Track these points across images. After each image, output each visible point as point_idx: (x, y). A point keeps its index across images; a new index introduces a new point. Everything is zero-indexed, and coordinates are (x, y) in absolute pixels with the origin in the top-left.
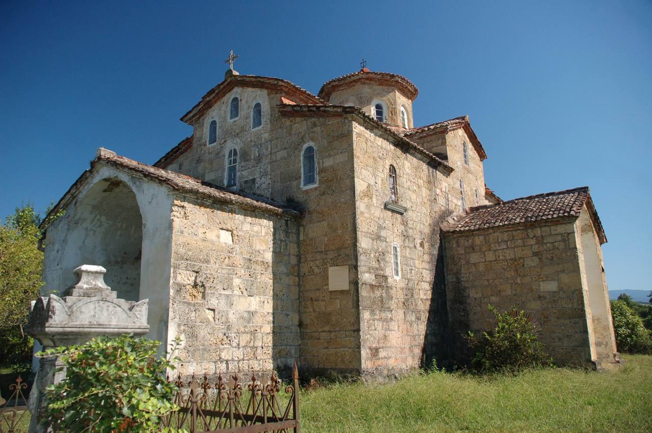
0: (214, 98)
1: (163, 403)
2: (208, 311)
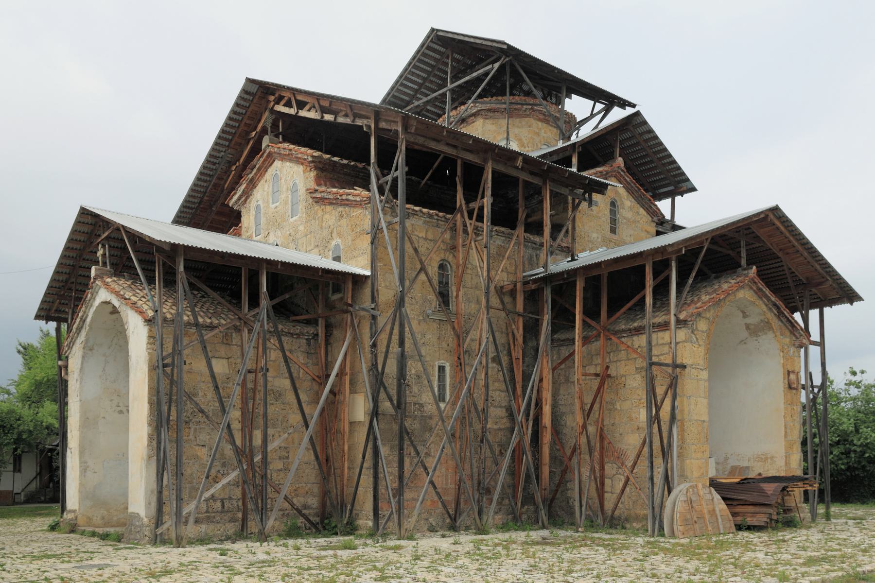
0: (256, 174)
1: (710, 492)
2: (197, 448)
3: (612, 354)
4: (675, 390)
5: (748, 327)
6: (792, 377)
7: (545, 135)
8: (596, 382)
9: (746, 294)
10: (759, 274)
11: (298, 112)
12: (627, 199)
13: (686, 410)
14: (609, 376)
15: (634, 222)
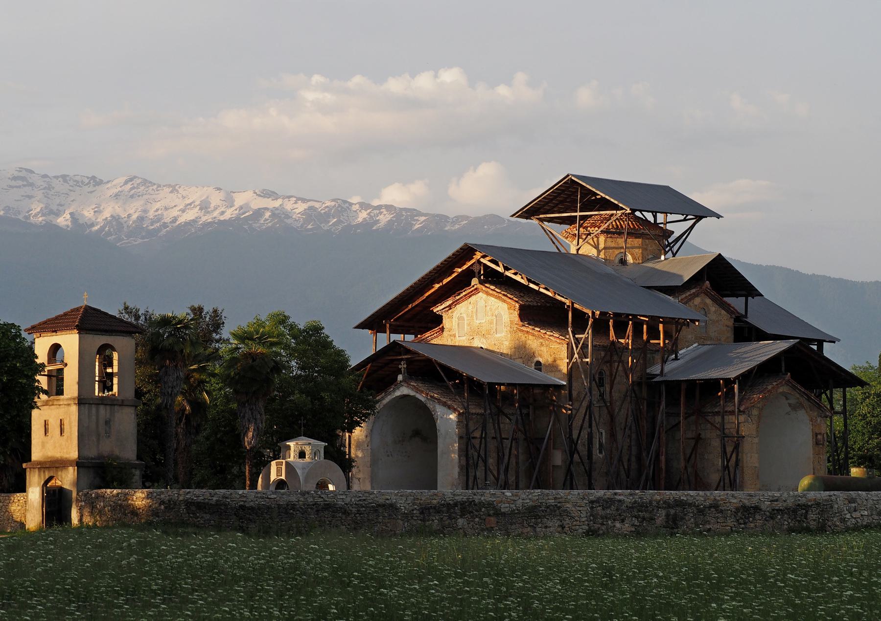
3: (702, 425)
4: (738, 449)
5: (790, 405)
6: (819, 437)
7: (651, 248)
8: (693, 443)
9: (784, 389)
10: (792, 377)
11: (505, 272)
12: (712, 306)
13: (745, 461)
14: (701, 439)
15: (717, 321)
